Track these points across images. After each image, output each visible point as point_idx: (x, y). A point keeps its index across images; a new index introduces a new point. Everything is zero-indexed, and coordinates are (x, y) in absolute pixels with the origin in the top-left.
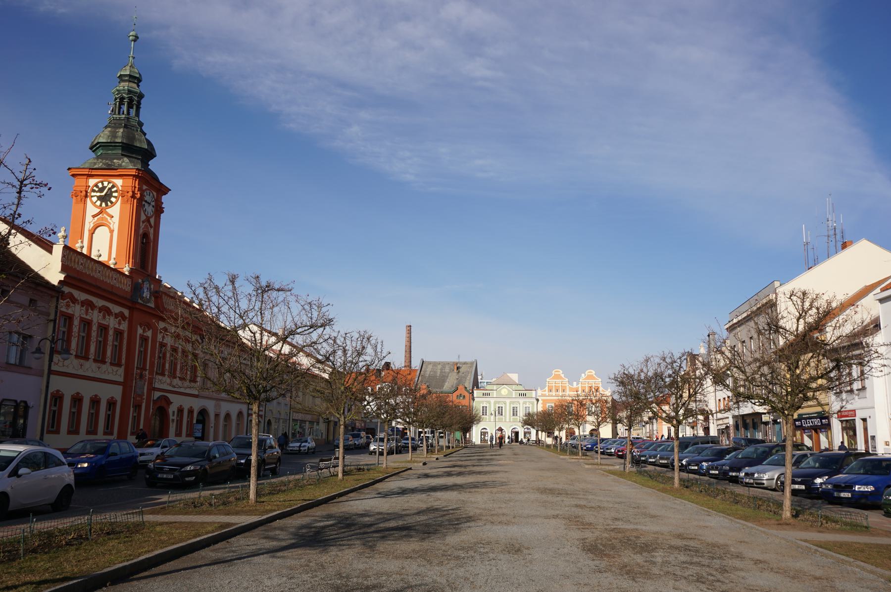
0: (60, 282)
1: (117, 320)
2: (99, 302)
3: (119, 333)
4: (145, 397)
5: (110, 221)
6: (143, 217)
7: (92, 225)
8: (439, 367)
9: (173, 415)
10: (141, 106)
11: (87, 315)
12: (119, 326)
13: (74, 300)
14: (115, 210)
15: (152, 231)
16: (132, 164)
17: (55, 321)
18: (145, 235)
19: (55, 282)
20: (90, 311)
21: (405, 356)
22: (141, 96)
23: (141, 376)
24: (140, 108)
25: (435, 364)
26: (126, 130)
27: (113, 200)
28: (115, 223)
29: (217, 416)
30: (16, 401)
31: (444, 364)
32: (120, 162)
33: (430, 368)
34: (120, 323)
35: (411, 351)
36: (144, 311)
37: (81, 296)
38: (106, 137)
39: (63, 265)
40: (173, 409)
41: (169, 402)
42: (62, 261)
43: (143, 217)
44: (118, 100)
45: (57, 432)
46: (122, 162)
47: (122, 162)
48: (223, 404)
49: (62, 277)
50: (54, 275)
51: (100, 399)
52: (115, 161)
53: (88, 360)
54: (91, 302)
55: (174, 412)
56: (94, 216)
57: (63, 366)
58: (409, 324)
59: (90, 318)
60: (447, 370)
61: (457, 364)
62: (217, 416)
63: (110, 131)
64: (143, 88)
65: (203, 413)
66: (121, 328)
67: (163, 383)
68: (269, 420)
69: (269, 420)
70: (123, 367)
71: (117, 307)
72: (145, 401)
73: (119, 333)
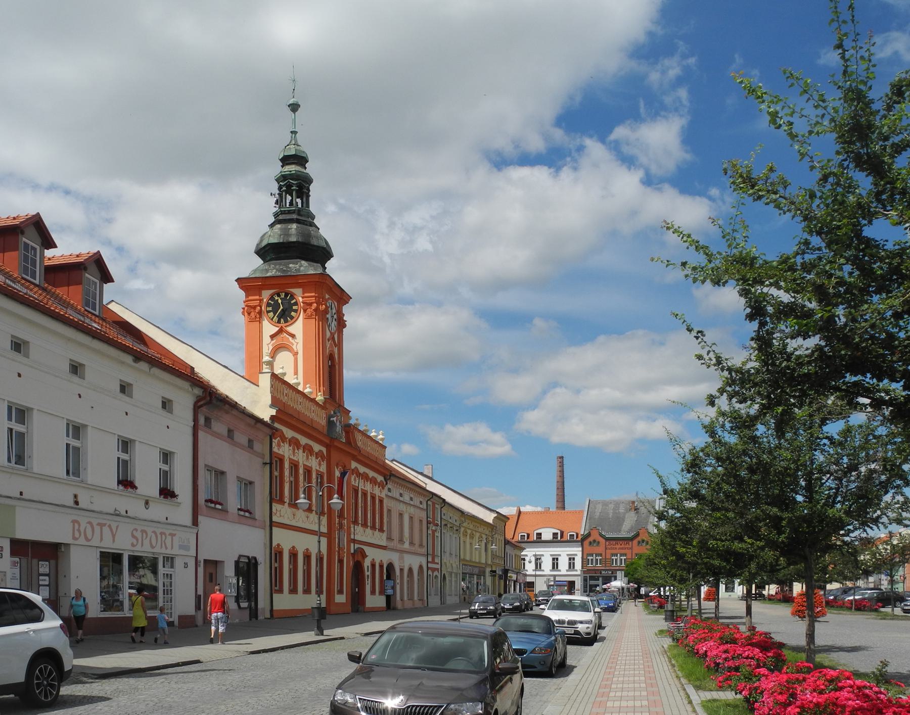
0: (272, 417)
1: (318, 460)
2: (304, 440)
3: (320, 475)
4: (345, 550)
5: (293, 341)
6: (328, 334)
7: (271, 348)
8: (612, 506)
9: (368, 571)
10: (310, 193)
11: (294, 455)
12: (320, 468)
13: (283, 439)
14: (297, 327)
15: (336, 350)
16: (312, 268)
17: (271, 464)
18: (331, 357)
19: (267, 419)
20: (296, 451)
21: (557, 495)
22: (308, 180)
23: (341, 526)
24: (310, 196)
25: (605, 504)
26: (299, 225)
27: (293, 314)
28: (298, 344)
29: (402, 570)
30: (248, 557)
31: (617, 504)
32: (297, 266)
33: (599, 508)
34: (320, 465)
35: (564, 489)
36: (341, 449)
37: (289, 433)
38: (276, 236)
39: (273, 398)
40: (367, 563)
41: (364, 556)
42: (271, 393)
43: (328, 334)
44: (284, 188)
45: (281, 591)
46: (300, 267)
47: (300, 267)
48: (406, 556)
49: (273, 412)
50: (265, 412)
51: (283, 549)
52: (291, 265)
53: (312, 513)
54: (297, 440)
55: (368, 567)
56: (272, 337)
57: (281, 516)
58: (561, 455)
59: (297, 460)
60: (622, 510)
61: (633, 502)
62: (402, 570)
63: (280, 229)
64: (311, 169)
65: (390, 567)
66: (321, 470)
67: (361, 534)
68: (444, 574)
69: (444, 574)
70: (326, 515)
71: (318, 445)
72: (345, 554)
73: (320, 475)
